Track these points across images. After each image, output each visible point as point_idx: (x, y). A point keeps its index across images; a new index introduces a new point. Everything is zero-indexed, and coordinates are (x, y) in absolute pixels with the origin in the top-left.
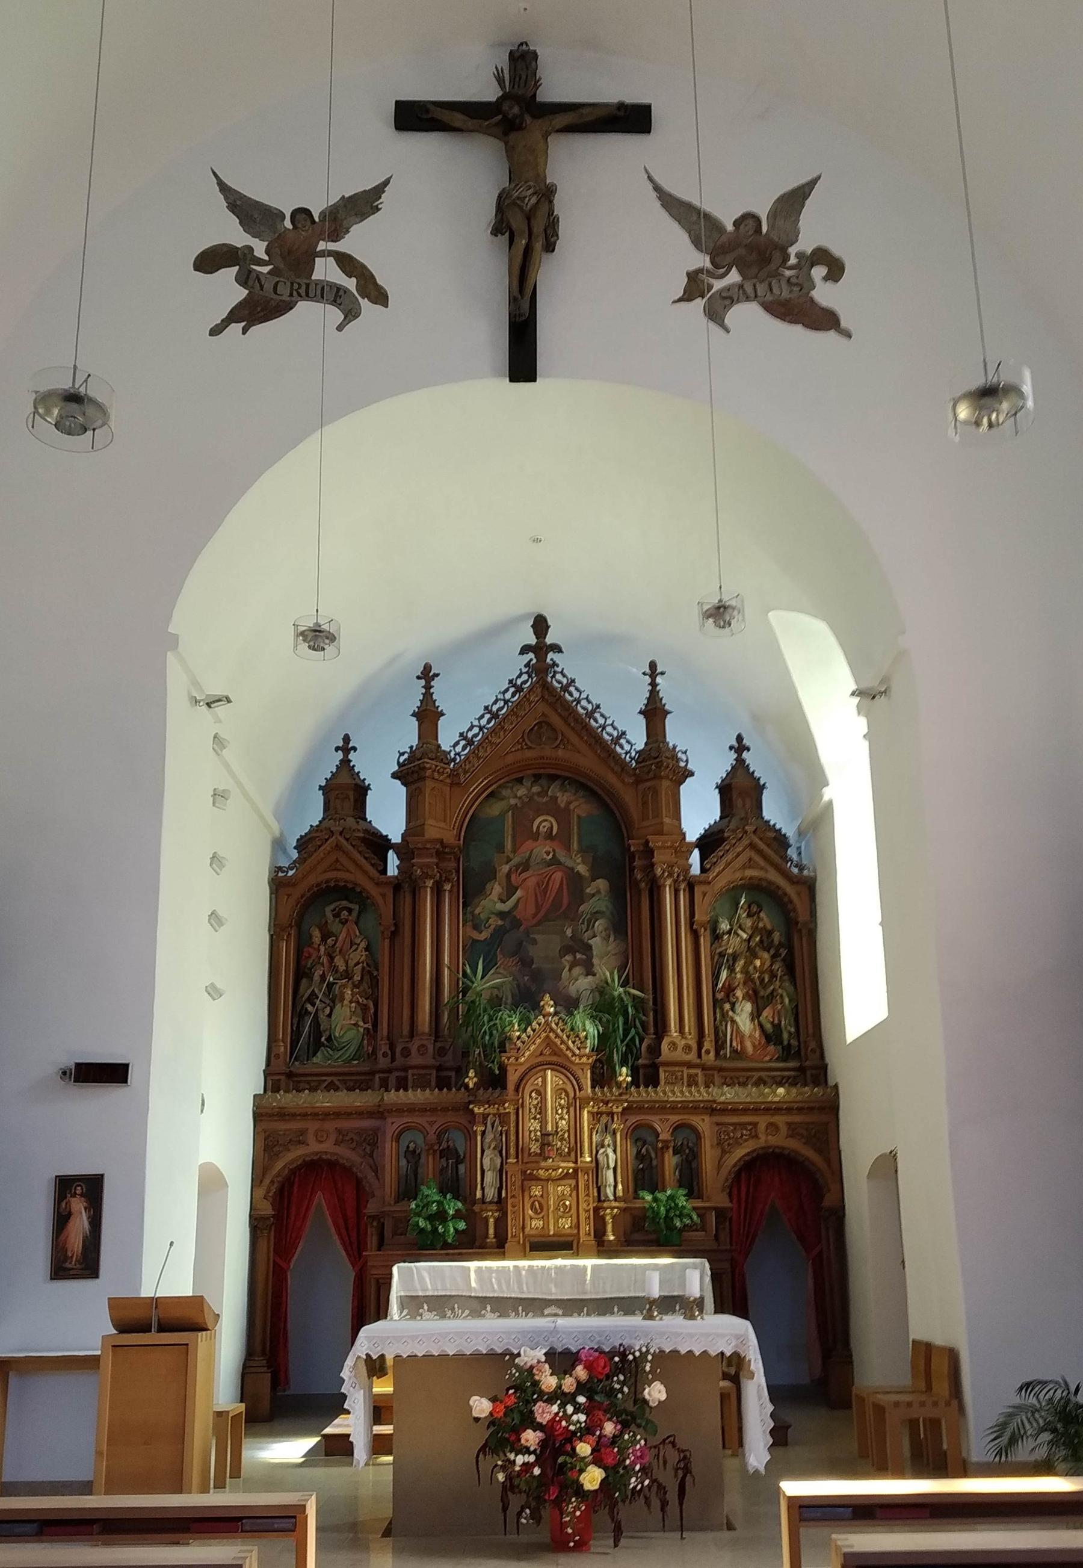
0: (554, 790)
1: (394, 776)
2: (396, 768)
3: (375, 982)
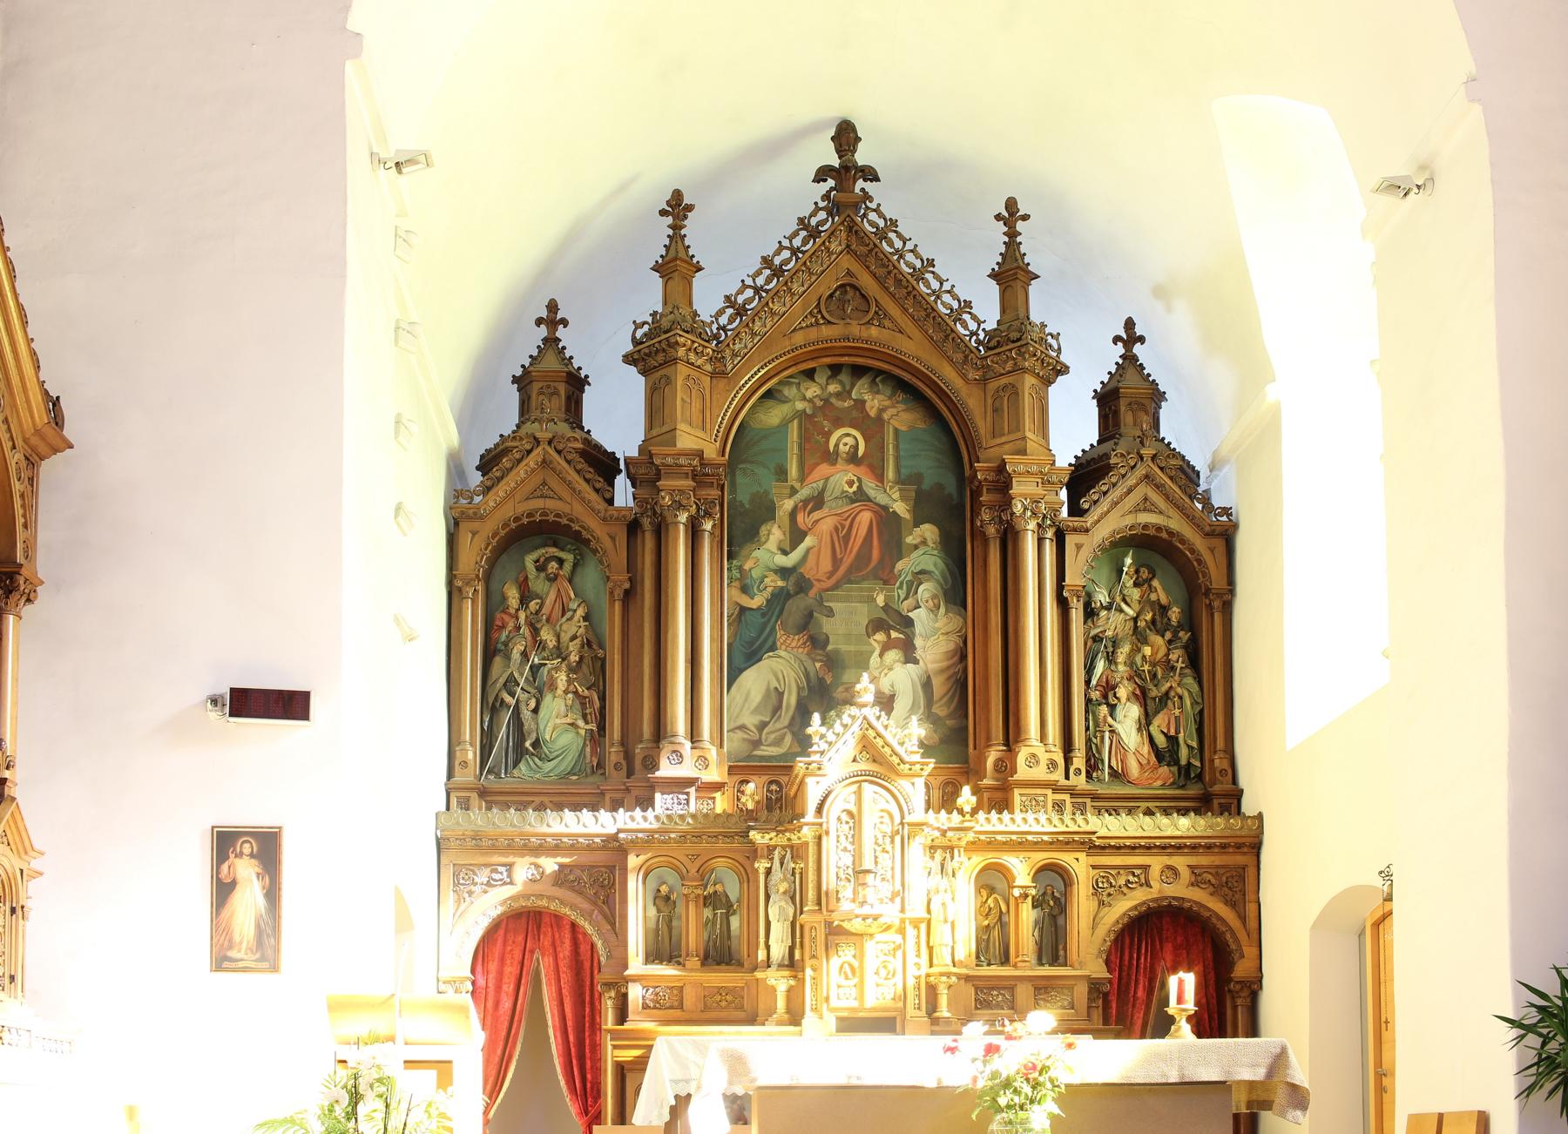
0: (861, 390)
1: (629, 359)
2: (630, 347)
3: (601, 667)
